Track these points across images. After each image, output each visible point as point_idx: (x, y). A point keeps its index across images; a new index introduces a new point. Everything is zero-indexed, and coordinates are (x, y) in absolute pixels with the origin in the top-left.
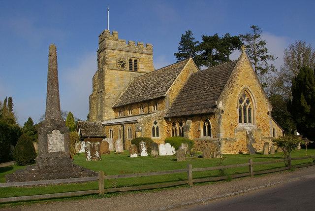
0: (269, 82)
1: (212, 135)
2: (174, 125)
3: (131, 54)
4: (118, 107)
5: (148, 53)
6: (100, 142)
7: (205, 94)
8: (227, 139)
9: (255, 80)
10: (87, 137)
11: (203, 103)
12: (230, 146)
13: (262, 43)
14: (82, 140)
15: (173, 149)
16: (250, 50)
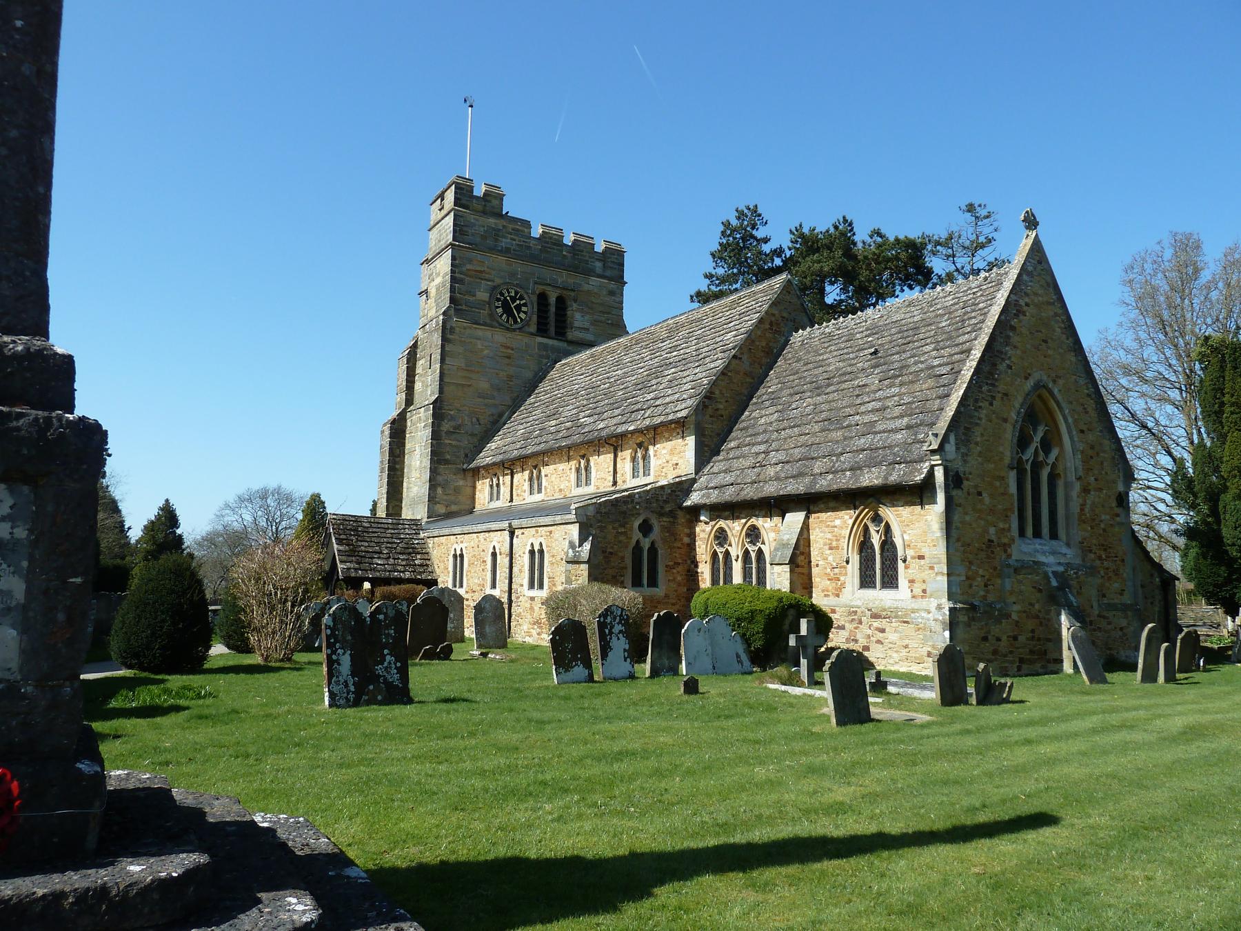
1: (902, 581)
3: (548, 273)
5: (608, 273)
7: (863, 409)
12: (985, 639)
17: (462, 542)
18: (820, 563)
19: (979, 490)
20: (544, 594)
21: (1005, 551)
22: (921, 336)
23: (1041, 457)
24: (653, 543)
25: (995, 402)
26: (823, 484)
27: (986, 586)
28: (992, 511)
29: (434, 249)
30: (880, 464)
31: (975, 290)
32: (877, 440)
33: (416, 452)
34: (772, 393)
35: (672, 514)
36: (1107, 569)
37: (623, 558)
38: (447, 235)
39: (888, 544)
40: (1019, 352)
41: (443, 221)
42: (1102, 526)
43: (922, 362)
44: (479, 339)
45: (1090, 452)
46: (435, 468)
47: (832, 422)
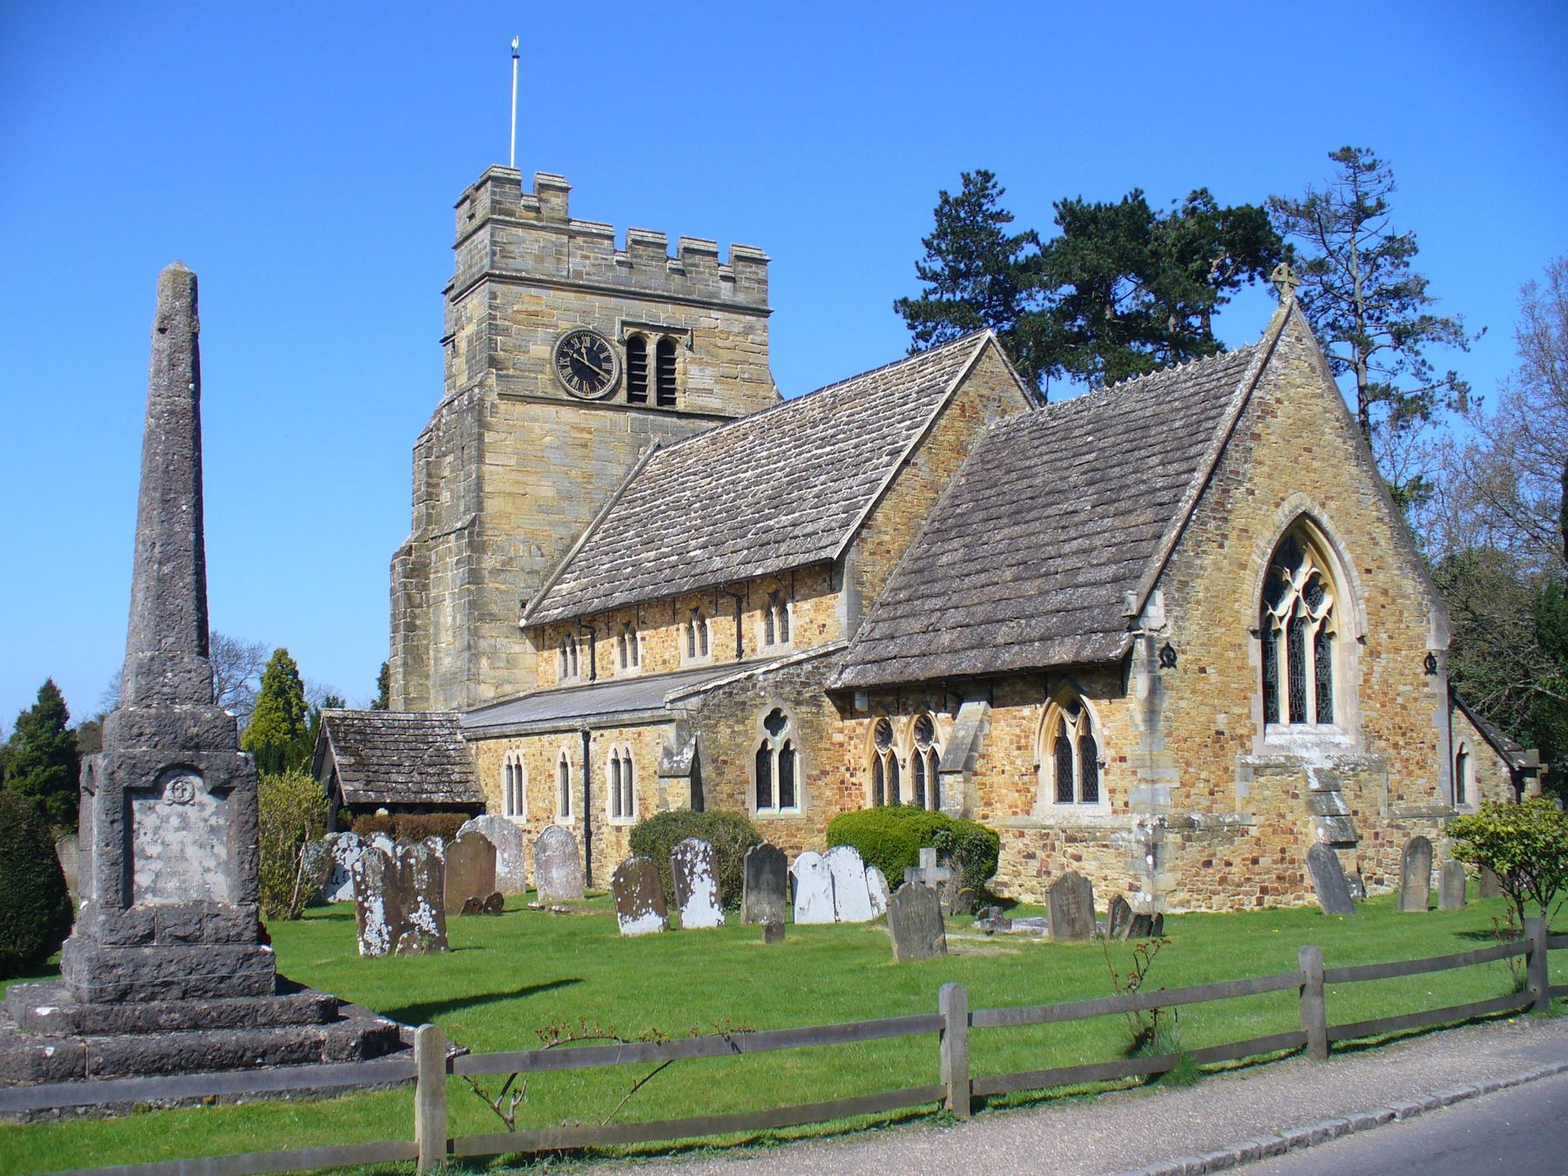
0: (1436, 473)
1: (1103, 792)
2: (885, 735)
4: (557, 624)
5: (741, 299)
6: (448, 836)
7: (1067, 548)
8: (1190, 824)
9: (1351, 469)
10: (371, 808)
11: (1057, 599)
12: (1208, 864)
13: (1397, 249)
14: (342, 827)
15: (875, 881)
16: (1328, 288)
17: (518, 747)
18: (1007, 768)
19: (1202, 664)
20: (633, 821)
21: (1242, 745)
22: (1151, 441)
23: (1303, 612)
24: (787, 744)
25: (1227, 543)
26: (1010, 659)
27: (1212, 793)
28: (1222, 693)
29: (462, 278)
30: (1074, 633)
31: (1220, 375)
32: (1076, 596)
33: (446, 603)
34: (962, 515)
35: (815, 701)
36: (1407, 760)
37: (742, 768)
38: (481, 258)
39: (1088, 744)
40: (1266, 469)
41: (475, 237)
42: (1400, 700)
43: (1144, 482)
44: (537, 420)
45: (1382, 599)
46: (476, 628)
47: (1028, 568)
